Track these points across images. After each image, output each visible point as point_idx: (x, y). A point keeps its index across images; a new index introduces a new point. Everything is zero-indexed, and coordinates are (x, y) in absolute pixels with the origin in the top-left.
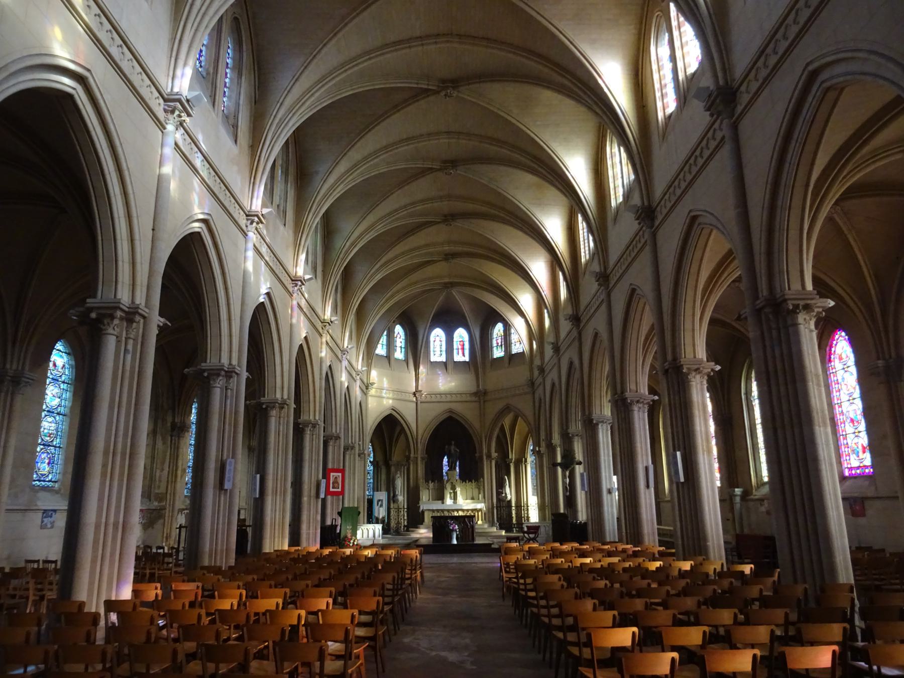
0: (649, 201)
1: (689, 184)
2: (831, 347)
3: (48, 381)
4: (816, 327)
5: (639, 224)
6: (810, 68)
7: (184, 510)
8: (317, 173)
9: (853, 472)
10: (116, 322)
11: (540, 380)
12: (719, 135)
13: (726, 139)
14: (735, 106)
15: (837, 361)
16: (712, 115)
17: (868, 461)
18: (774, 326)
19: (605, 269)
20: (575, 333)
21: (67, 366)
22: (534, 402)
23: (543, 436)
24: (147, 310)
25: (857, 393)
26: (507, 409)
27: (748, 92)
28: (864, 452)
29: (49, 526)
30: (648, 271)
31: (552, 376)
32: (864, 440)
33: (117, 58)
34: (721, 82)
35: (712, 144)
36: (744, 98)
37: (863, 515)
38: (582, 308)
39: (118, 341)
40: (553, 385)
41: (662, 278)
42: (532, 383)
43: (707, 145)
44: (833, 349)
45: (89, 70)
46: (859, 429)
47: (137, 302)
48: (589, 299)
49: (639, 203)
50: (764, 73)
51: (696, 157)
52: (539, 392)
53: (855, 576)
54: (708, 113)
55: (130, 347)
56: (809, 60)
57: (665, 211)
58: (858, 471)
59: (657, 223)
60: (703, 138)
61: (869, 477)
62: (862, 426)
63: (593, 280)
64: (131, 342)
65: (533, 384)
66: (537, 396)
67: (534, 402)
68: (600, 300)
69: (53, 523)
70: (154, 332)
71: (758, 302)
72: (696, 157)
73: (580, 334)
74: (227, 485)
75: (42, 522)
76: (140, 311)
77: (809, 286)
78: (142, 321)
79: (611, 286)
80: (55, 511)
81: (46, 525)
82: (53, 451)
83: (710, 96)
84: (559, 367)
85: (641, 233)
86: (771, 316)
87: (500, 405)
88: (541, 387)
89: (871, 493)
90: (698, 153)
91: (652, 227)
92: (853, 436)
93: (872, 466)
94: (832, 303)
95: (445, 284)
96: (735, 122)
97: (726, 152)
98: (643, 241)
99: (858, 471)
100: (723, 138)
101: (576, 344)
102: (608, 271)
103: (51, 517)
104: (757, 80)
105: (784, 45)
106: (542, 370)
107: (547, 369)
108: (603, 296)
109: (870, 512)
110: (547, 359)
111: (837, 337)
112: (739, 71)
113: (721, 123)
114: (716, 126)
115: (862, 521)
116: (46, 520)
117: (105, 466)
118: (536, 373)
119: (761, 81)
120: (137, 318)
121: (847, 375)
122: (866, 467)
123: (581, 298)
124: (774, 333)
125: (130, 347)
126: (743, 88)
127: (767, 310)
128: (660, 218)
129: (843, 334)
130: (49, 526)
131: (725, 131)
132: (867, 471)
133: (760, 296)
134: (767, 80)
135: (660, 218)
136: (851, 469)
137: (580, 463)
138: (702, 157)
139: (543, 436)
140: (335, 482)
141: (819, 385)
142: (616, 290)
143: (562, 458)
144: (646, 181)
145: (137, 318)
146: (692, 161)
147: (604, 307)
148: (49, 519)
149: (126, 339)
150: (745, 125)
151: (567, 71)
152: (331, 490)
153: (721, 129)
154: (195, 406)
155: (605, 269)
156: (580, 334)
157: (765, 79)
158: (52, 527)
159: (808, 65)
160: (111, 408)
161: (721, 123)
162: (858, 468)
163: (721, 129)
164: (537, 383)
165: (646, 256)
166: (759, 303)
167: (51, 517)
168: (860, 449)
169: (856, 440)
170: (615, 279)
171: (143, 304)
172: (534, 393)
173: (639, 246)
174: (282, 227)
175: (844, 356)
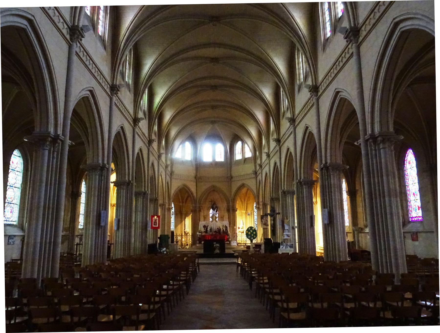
0: (316, 82)
1: (333, 78)
2: (405, 157)
3: (10, 170)
4: (395, 149)
5: (311, 94)
6: (336, 90)
7: (78, 236)
8: (146, 64)
9: (413, 219)
10: (48, 143)
11: (260, 171)
12: (351, 52)
13: (354, 54)
14: (359, 37)
15: (408, 164)
16: (347, 41)
17: (420, 214)
18: (326, 174)
19: (293, 116)
20: (278, 148)
21: (19, 163)
22: (257, 182)
23: (261, 200)
24: (63, 137)
25: (416, 181)
26: (243, 185)
27: (379, 12)
28: (419, 209)
29: (12, 243)
30: (315, 118)
31: (266, 169)
32: (419, 203)
33: (52, 16)
34: (352, 25)
35: (347, 56)
36: (364, 33)
37: (417, 240)
38: (281, 135)
39: (49, 153)
40: (266, 174)
41: (363, 76)
42: (256, 173)
43: (345, 56)
44: (406, 158)
45: (34, 16)
46: (417, 198)
47: (152, 206)
48: (285, 131)
49: (311, 84)
50: (373, 21)
51: (339, 62)
52: (259, 177)
53: (408, 269)
54: (310, 93)
55: (55, 156)
56: (395, 17)
57: (323, 88)
58: (416, 219)
59: (319, 94)
60: (340, 57)
61: (421, 222)
62: (418, 197)
63: (287, 121)
64: (56, 153)
65: (256, 173)
66: (258, 179)
67: (257, 182)
68: (290, 132)
69: (14, 242)
70: (67, 148)
71: (366, 137)
72: (339, 62)
73: (280, 148)
74: (102, 224)
75: (9, 241)
76: (60, 138)
77: (391, 129)
78: (61, 142)
79: (360, 41)
80: (15, 236)
81: (10, 243)
82: (13, 206)
83: (347, 31)
84: (270, 166)
85: (311, 99)
86: (372, 143)
87: (240, 183)
88: (260, 174)
89: (421, 229)
90: (340, 59)
91: (357, 43)
92: (414, 201)
93: (422, 217)
94: (402, 137)
95: (212, 121)
96: (358, 45)
97: (353, 61)
98: (312, 102)
99: (416, 219)
100: (352, 53)
101: (278, 153)
102: (295, 117)
103: (13, 239)
104: (370, 25)
105: (378, 15)
106: (261, 166)
107: (271, 155)
108: (292, 130)
109: (420, 239)
110: (263, 161)
111: (408, 152)
112: (361, 20)
113: (352, 45)
114: (350, 46)
115: (417, 243)
116: (10, 240)
117: (44, 215)
118: (258, 167)
119: (371, 25)
120: (59, 141)
121: (412, 171)
122: (420, 217)
123: (281, 130)
124: (374, 152)
125: (55, 156)
126: (363, 28)
127: (371, 141)
128: (321, 91)
129: (411, 151)
130: (12, 243)
131: (353, 50)
132: (420, 219)
133: (368, 133)
134: (374, 25)
135: (321, 91)
136: (412, 218)
137: (279, 213)
138: (345, 58)
139: (261, 200)
140: (155, 222)
141: (394, 177)
142: (364, 44)
143: (270, 211)
144: (314, 72)
145: (59, 141)
146: (337, 64)
147: (292, 136)
148: (12, 240)
149: (53, 152)
150: (363, 48)
151: (277, 15)
152: (157, 226)
153: (352, 48)
154: (83, 183)
155: (293, 116)
156: (280, 148)
157: (374, 24)
158: (13, 244)
159: (394, 19)
160: (46, 185)
161: (352, 45)
162: (416, 217)
163: (352, 48)
164: (258, 173)
165: (313, 111)
166: (367, 137)
167: (13, 239)
168: (417, 208)
169: (415, 204)
170: (299, 121)
171: (61, 134)
172: (257, 178)
173: (311, 105)
174: (128, 92)
175: (411, 162)
